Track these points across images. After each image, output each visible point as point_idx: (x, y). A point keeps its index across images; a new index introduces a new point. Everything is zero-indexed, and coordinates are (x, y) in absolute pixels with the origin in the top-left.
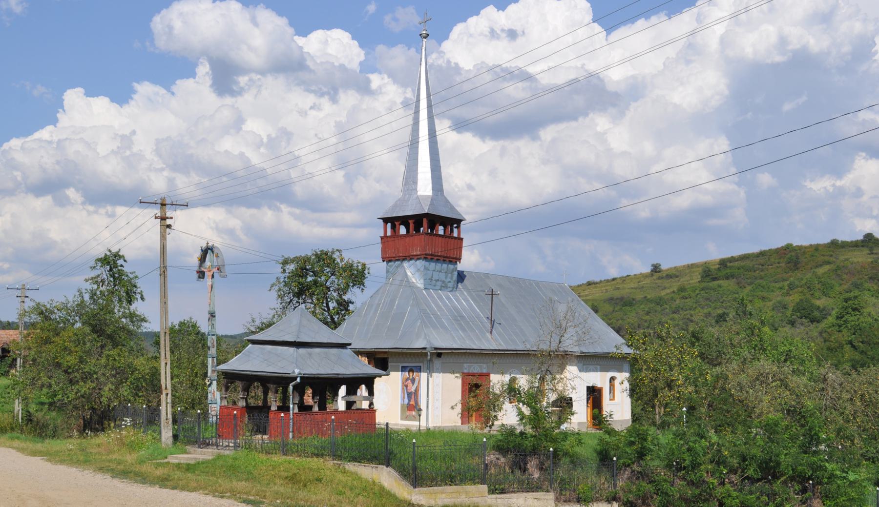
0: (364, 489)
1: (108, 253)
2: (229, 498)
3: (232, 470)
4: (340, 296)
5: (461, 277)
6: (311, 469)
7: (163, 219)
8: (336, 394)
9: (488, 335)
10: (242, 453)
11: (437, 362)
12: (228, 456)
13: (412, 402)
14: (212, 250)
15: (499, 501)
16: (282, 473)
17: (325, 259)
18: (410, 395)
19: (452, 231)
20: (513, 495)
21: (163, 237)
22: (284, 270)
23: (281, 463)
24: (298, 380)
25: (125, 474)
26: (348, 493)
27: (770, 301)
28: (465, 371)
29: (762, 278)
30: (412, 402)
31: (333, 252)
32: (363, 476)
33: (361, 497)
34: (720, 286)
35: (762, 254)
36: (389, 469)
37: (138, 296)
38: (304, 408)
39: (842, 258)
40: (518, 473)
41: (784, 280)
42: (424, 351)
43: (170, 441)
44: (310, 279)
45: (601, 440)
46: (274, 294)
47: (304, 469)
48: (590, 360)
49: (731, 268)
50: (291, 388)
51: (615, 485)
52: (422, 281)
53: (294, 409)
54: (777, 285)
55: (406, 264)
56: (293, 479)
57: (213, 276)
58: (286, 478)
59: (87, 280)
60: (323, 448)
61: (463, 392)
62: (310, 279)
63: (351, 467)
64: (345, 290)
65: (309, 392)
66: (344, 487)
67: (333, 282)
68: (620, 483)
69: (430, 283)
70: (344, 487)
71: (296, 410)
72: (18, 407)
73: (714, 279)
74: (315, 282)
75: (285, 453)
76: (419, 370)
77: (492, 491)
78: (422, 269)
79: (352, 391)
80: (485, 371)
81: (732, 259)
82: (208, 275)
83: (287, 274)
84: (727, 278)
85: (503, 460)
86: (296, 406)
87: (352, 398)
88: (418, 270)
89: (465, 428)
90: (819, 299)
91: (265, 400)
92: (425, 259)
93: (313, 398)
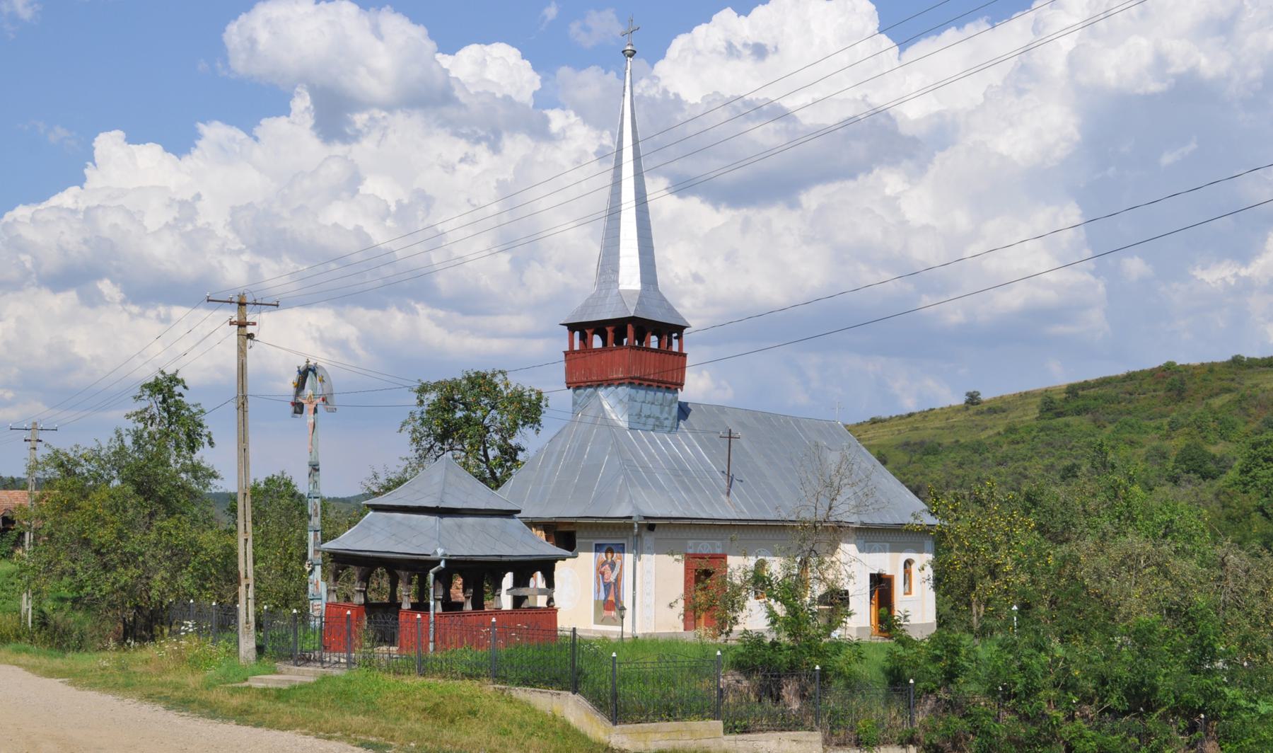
0: (540, 727)
1: (161, 376)
2: (339, 739)
3: (344, 698)
4: (505, 440)
5: (684, 411)
6: (460, 697)
7: (242, 325)
8: (498, 585)
9: (724, 497)
11: (648, 538)
12: (338, 677)
13: (611, 598)
14: (314, 371)
17: (481, 384)
18: (607, 586)
19: (670, 343)
20: (761, 735)
21: (242, 352)
23: (417, 688)
24: (442, 564)
25: (184, 703)
27: (1142, 447)
28: (690, 551)
29: (1129, 413)
30: (611, 598)
31: (494, 375)
32: (538, 708)
33: (535, 739)
36: (577, 697)
37: (205, 440)
38: (450, 606)
39: (1248, 383)
40: (768, 702)
41: (1162, 416)
42: (628, 521)
43: (252, 655)
44: (459, 414)
45: (891, 653)
46: (406, 436)
47: (451, 697)
48: (874, 536)
49: (1084, 397)
50: (431, 576)
51: (912, 721)
52: (626, 417)
53: (435, 607)
54: (1152, 424)
55: (602, 392)
56: (434, 712)
57: (315, 411)
58: (424, 710)
59: (128, 416)
60: (479, 665)
61: (686, 582)
62: (459, 414)
63: (521, 693)
64: (511, 431)
65: (458, 582)
67: (495, 418)
68: (920, 718)
69: (638, 420)
70: (511, 723)
71: (439, 610)
72: (26, 605)
73: (1059, 415)
74: (468, 419)
75: (980, 443)
76: (621, 549)
77: (729, 730)
78: (626, 400)
79: (521, 580)
80: (719, 551)
81: (1086, 385)
82: (308, 408)
83: (425, 408)
84: (1079, 413)
85: (745, 683)
86: (439, 604)
87: (522, 592)
88: (621, 401)
89: (690, 636)
90: (1215, 443)
92: (631, 384)
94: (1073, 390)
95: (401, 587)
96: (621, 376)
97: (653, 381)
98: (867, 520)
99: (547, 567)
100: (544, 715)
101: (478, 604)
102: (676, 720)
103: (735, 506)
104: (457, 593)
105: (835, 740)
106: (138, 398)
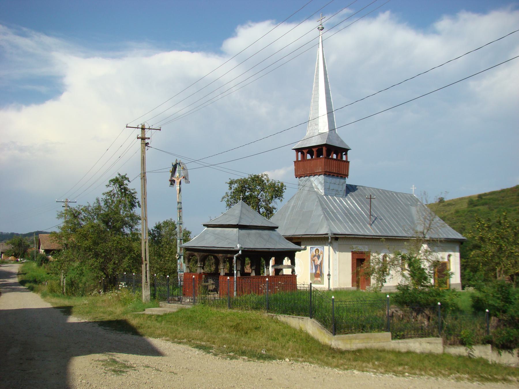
1: (118, 176)
3: (189, 319)
4: (267, 205)
6: (250, 320)
7: (143, 139)
8: (268, 264)
10: (199, 307)
12: (188, 309)
13: (318, 272)
15: (401, 345)
16: (229, 323)
17: (257, 180)
18: (316, 267)
19: (342, 157)
21: (143, 152)
22: (231, 188)
23: (227, 315)
24: (240, 252)
26: (281, 339)
28: (354, 250)
29: (503, 205)
33: (291, 343)
34: (479, 210)
35: (503, 191)
37: (137, 204)
38: (244, 274)
42: (326, 236)
45: (473, 297)
48: (437, 243)
49: (485, 199)
50: (235, 258)
51: (487, 332)
54: (512, 209)
55: (312, 178)
56: (236, 328)
57: (180, 182)
58: (231, 327)
61: (353, 264)
63: (283, 318)
64: (268, 202)
65: (247, 260)
66: (278, 334)
67: (263, 196)
69: (328, 191)
70: (278, 334)
71: (239, 275)
73: (476, 206)
74: (251, 196)
75: (230, 307)
77: (395, 337)
78: (323, 182)
79: (279, 262)
81: (485, 195)
82: (177, 181)
83: (232, 190)
86: (239, 272)
87: (280, 267)
91: (217, 269)
93: (251, 267)
94: (480, 197)
95: (221, 266)
96: (320, 171)
97: (335, 173)
98: (433, 236)
99: (291, 255)
100: (295, 329)
101: (258, 273)
102: (366, 332)
103: (374, 229)
104: (248, 269)
105: (449, 342)
106: (108, 186)
